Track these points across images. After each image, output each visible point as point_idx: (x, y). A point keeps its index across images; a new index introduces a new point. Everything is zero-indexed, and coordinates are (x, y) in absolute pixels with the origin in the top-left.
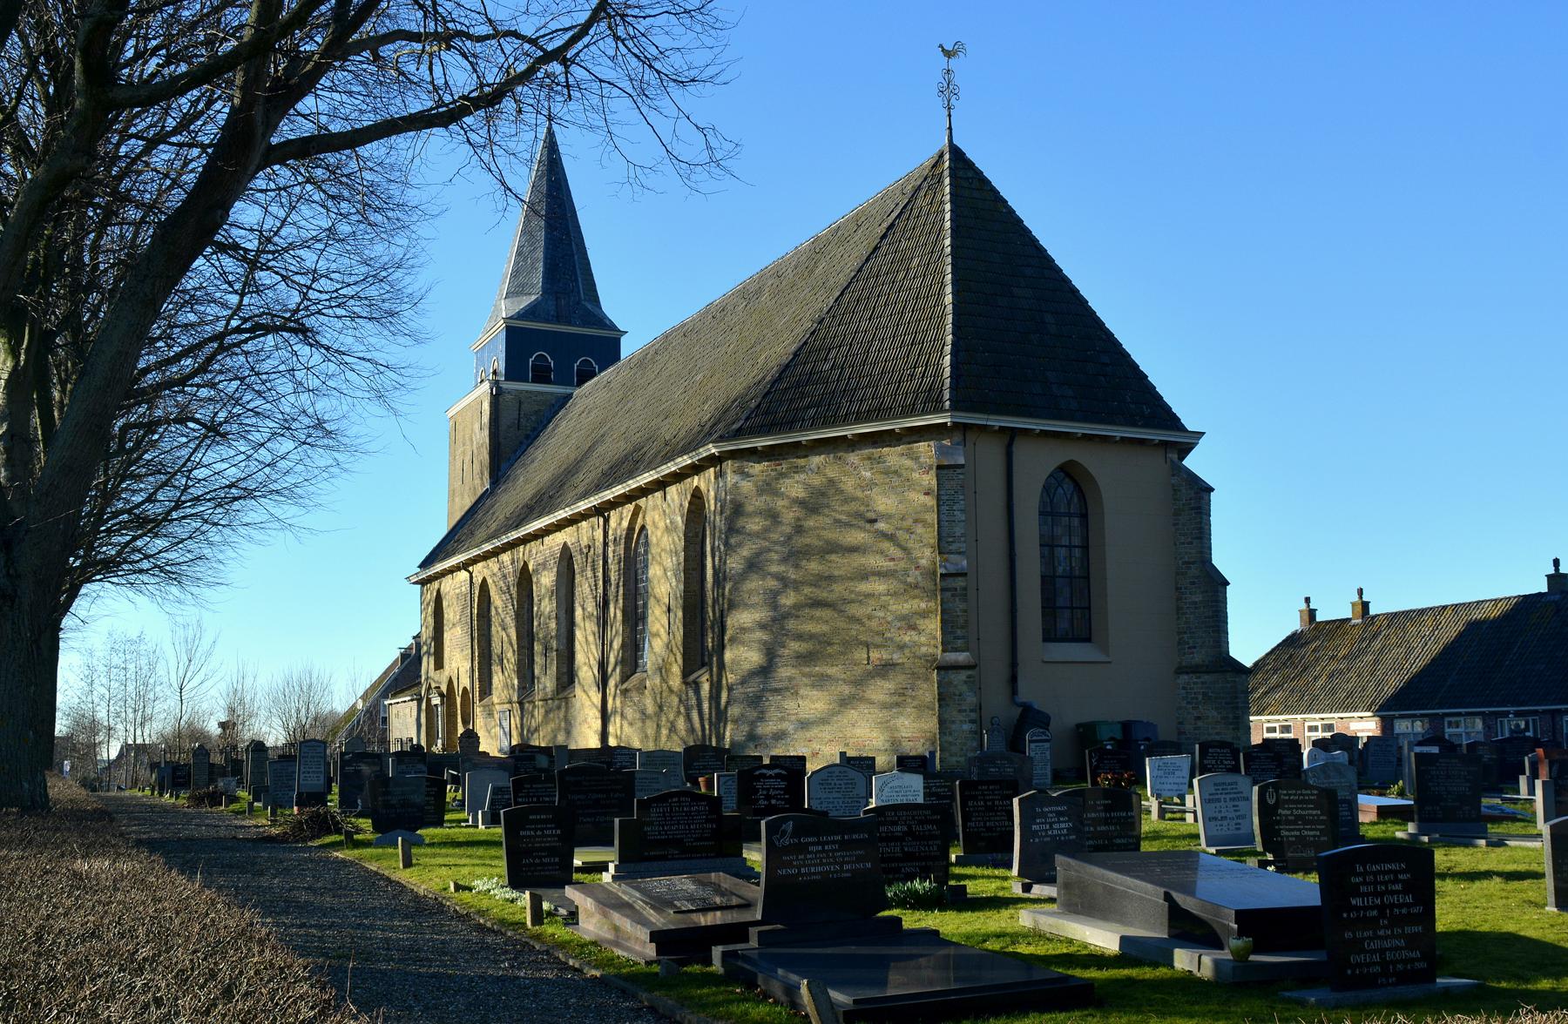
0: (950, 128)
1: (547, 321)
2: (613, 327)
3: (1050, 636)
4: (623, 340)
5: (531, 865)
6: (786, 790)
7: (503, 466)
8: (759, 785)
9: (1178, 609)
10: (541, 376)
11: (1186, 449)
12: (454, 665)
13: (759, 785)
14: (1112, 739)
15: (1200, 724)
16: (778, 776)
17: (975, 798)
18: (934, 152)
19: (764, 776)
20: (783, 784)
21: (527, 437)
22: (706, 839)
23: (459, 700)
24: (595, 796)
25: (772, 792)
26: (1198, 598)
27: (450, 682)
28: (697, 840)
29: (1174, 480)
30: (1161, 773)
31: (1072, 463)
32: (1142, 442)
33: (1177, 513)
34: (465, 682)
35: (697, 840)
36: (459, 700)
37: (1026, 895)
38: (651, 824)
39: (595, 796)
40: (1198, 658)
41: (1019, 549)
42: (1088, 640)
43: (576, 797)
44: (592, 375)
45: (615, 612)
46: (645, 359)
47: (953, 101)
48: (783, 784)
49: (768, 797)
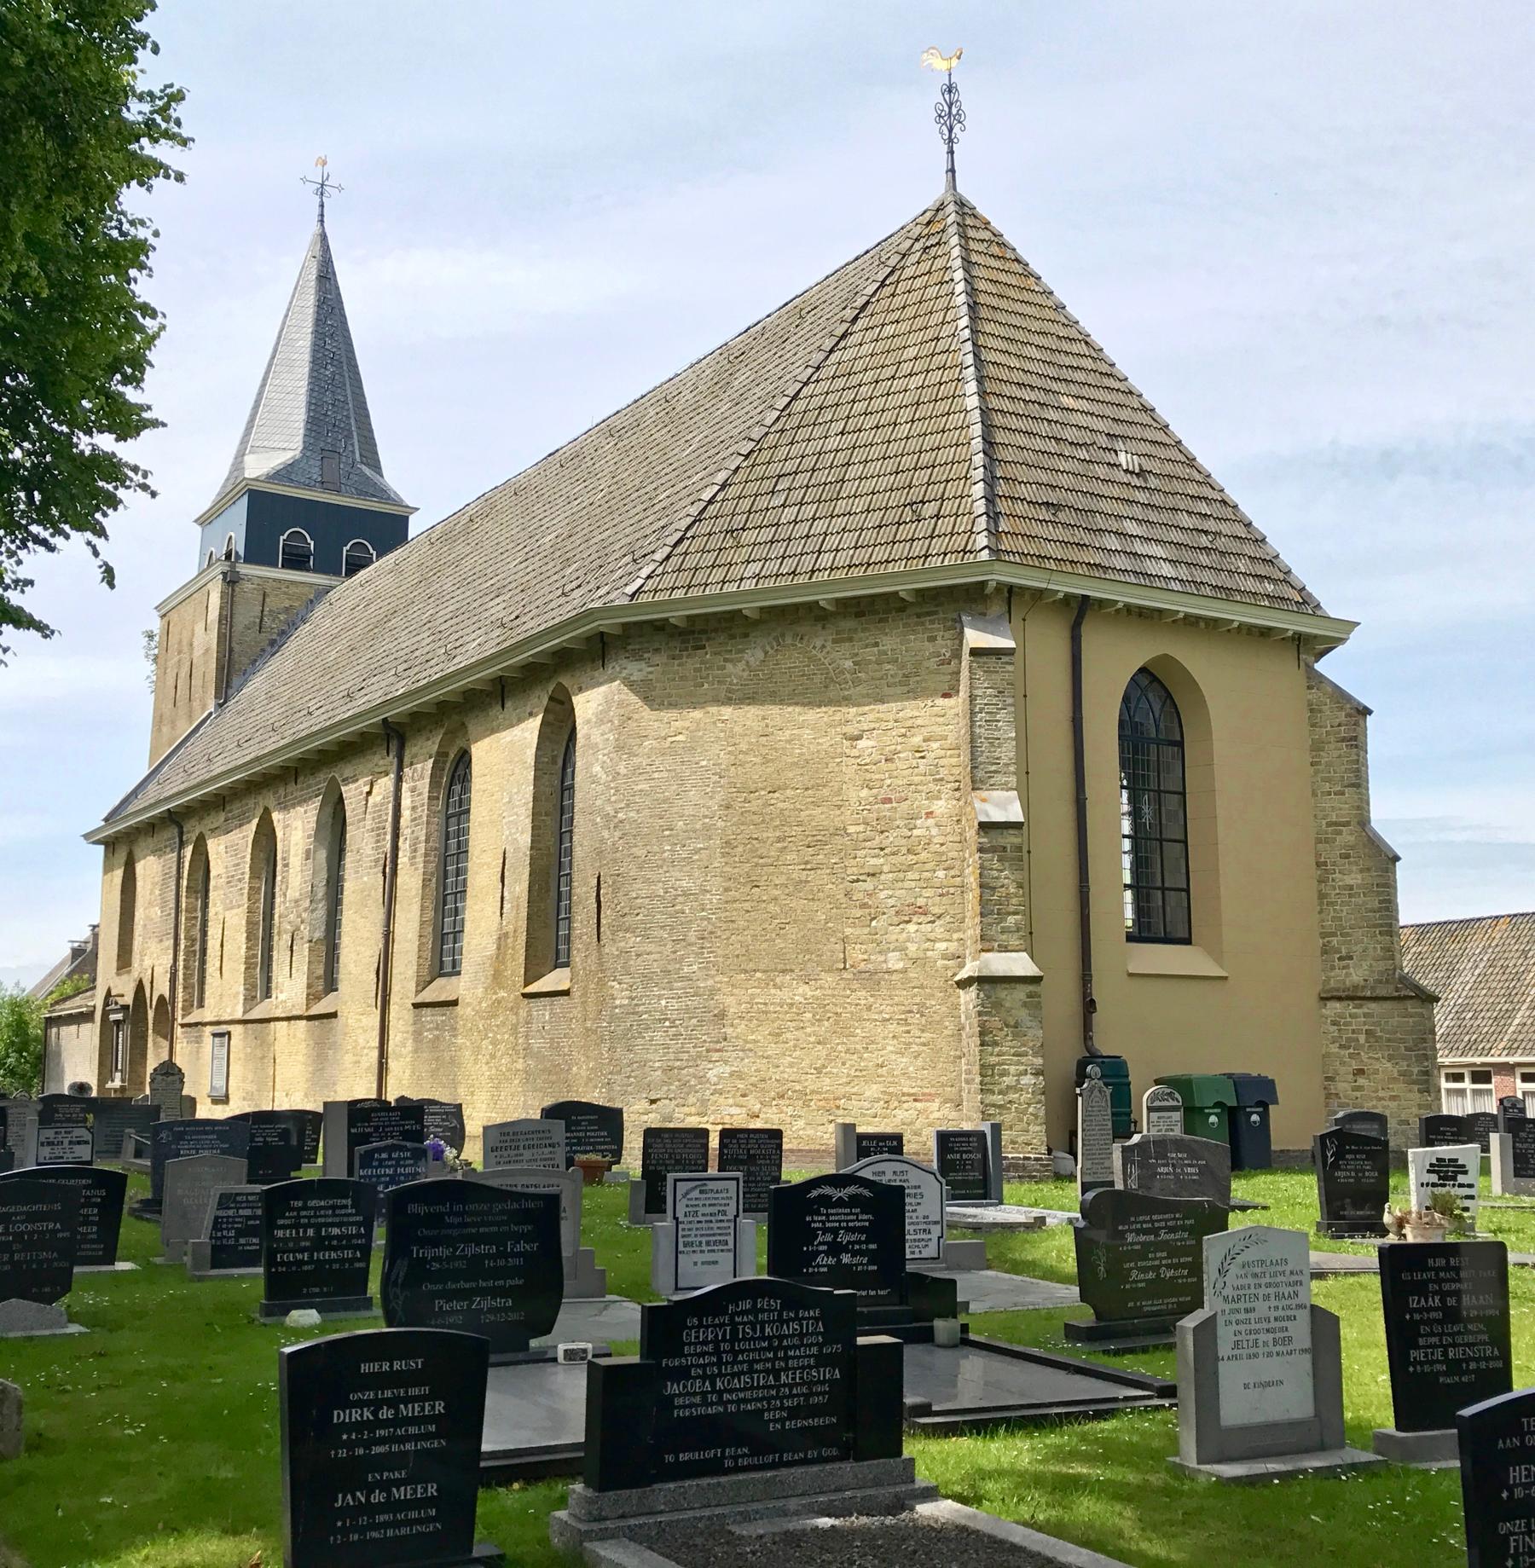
0: (952, 171)
1: (308, 487)
2: (399, 503)
3: (1142, 934)
4: (412, 519)
5: (361, 1509)
6: (872, 1232)
7: (236, 681)
8: (816, 1222)
9: (1322, 896)
10: (296, 560)
11: (1325, 645)
12: (148, 963)
13: (816, 1222)
14: (1218, 1104)
15: (1361, 1081)
16: (854, 1201)
17: (1421, 1289)
18: (930, 202)
19: (825, 1201)
20: (865, 1219)
21: (272, 643)
22: (815, 1411)
23: (151, 1014)
24: (472, 1250)
25: (844, 1238)
26: (1354, 879)
27: (140, 987)
28: (794, 1413)
29: (1314, 695)
30: (1434, 1178)
31: (1166, 659)
32: (1265, 633)
33: (1317, 747)
34: (163, 988)
35: (794, 1413)
36: (151, 1014)
37: (1187, 1393)
38: (683, 1374)
39: (472, 1250)
40: (1356, 975)
41: (397, 947)
42: (1187, 941)
43: (429, 1253)
44: (366, 563)
45: (410, 880)
46: (462, 527)
47: (956, 130)
48: (865, 1219)
49: (835, 1249)
